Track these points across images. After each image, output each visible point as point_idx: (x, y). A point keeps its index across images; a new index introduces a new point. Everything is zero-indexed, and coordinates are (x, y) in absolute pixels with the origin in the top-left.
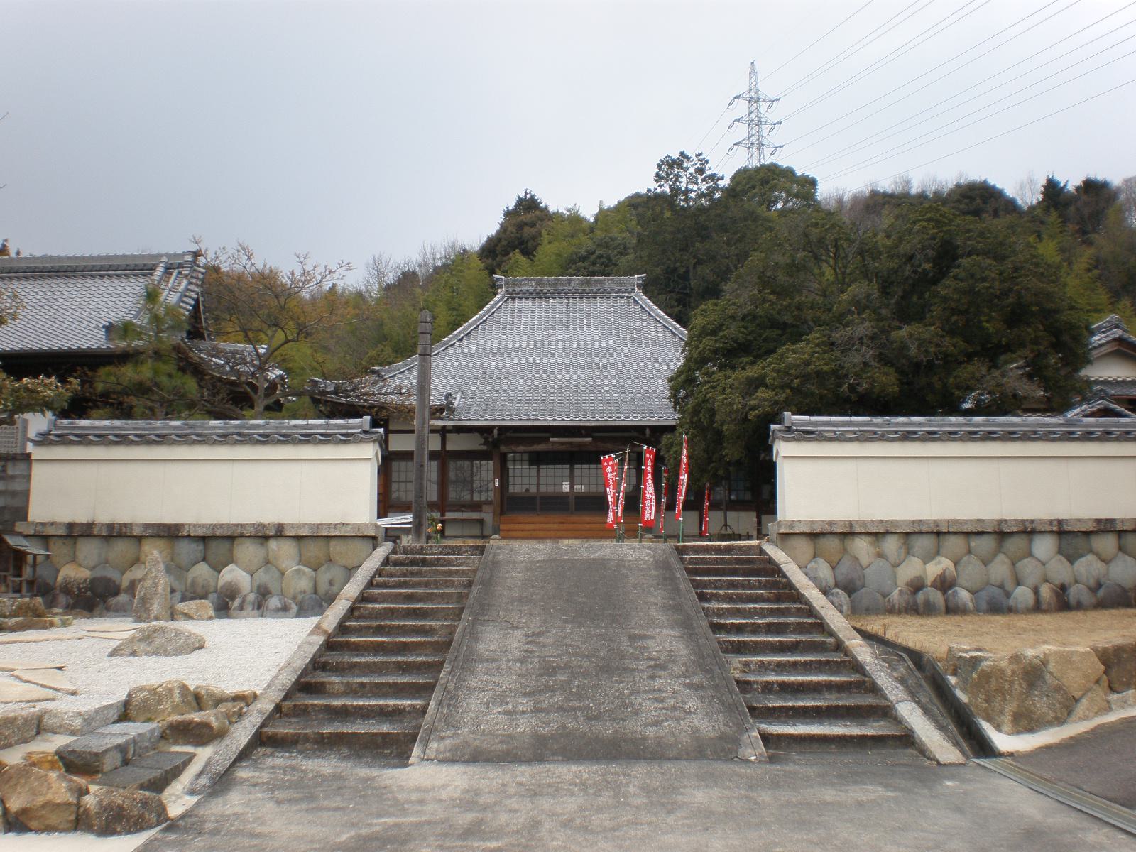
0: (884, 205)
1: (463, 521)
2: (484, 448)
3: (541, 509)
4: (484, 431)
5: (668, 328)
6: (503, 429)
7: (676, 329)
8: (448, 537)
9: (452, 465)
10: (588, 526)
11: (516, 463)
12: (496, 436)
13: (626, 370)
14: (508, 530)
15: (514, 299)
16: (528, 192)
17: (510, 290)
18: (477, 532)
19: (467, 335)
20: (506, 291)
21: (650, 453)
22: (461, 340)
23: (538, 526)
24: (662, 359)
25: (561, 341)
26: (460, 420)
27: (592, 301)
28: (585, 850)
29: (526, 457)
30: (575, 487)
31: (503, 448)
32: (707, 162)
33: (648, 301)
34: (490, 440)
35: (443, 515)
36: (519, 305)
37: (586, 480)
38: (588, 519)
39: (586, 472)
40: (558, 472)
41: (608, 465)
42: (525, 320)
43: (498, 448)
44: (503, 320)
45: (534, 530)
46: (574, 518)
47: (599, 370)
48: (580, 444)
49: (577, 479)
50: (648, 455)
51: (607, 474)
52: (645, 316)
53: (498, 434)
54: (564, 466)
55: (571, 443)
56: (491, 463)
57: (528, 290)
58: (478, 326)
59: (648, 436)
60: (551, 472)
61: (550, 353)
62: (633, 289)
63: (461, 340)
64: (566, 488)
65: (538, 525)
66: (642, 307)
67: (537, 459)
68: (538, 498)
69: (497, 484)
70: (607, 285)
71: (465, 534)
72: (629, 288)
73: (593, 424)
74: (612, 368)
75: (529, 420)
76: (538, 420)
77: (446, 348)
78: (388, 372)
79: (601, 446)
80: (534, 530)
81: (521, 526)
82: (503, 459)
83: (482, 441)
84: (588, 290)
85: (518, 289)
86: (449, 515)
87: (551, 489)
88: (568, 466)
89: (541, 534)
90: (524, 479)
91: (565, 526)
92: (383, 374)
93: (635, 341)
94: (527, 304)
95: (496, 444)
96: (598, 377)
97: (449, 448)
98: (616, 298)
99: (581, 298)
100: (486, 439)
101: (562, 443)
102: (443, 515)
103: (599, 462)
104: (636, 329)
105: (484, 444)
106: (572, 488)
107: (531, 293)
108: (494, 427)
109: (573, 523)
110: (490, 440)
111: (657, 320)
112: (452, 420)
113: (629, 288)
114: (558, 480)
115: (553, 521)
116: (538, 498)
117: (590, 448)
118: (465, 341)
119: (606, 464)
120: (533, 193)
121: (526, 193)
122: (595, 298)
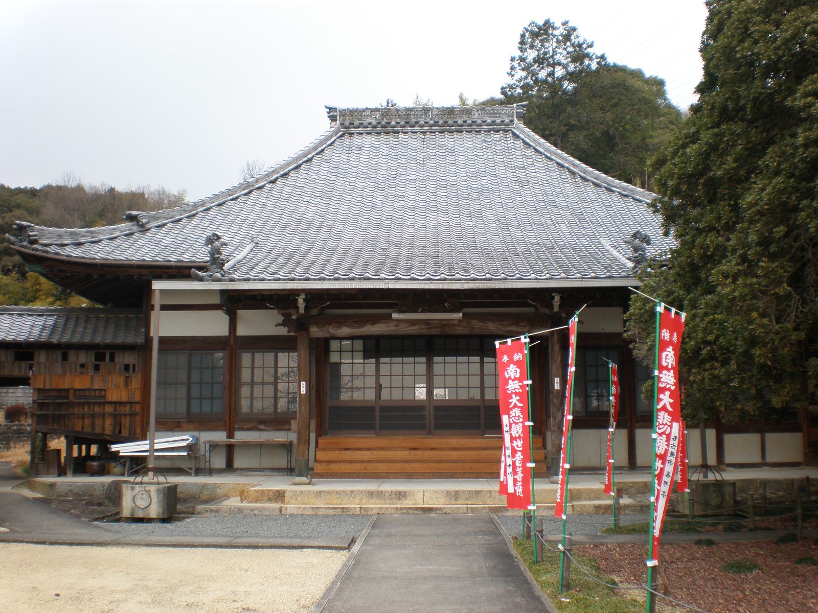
0: (699, 131)
1: (261, 446)
2: (283, 331)
3: (384, 427)
4: (280, 300)
5: (562, 166)
6: (314, 297)
7: (575, 166)
8: (238, 469)
9: (246, 358)
10: (454, 454)
11: (355, 353)
12: (302, 311)
13: (510, 215)
14: (330, 462)
15: (351, 134)
16: (390, 101)
17: (347, 123)
18: (282, 462)
19: (283, 176)
20: (342, 124)
21: (673, 325)
22: (273, 182)
23: (376, 454)
24: (561, 202)
25: (415, 181)
26: (232, 280)
27: (455, 135)
28: (438, 608)
29: (359, 344)
30: (436, 391)
31: (315, 331)
32: (574, 29)
33: (532, 133)
34: (294, 317)
35: (230, 435)
36: (357, 140)
37: (451, 381)
38: (454, 441)
39: (451, 369)
40: (409, 369)
41: (511, 361)
42: (364, 158)
43: (307, 330)
44: (335, 158)
45: (369, 461)
46: (433, 441)
47: (470, 216)
48: (443, 324)
49: (437, 380)
50: (666, 334)
51: (506, 381)
52: (530, 152)
53: (306, 308)
54: (418, 359)
55: (426, 322)
56: (294, 355)
57: (370, 123)
58: (300, 166)
59: (556, 309)
60: (397, 369)
61: (397, 195)
62: (512, 121)
63: (273, 182)
64: (421, 393)
65: (375, 453)
66: (525, 142)
67: (377, 348)
68: (377, 410)
69: (303, 391)
70: (476, 116)
71: (264, 466)
72: (507, 120)
73: (467, 286)
74: (487, 213)
75: (353, 279)
76: (369, 279)
77: (250, 192)
78: (155, 218)
79: (492, 327)
80: (369, 461)
81: (349, 455)
82: (321, 349)
83: (280, 319)
84: (450, 122)
85: (356, 123)
86: (240, 436)
87: (397, 395)
88: (424, 359)
89: (382, 467)
90: (361, 379)
91: (419, 454)
92: (144, 221)
93: (519, 181)
94: (368, 140)
95: (301, 325)
96: (468, 224)
97: (242, 331)
98: (489, 131)
99: (442, 132)
100: (287, 317)
101: (413, 322)
102: (230, 435)
103: (493, 353)
104: (519, 168)
105: (284, 324)
106: (430, 393)
107: (375, 127)
108: (295, 293)
109: (432, 449)
110: (294, 317)
111: (547, 157)
112: (219, 280)
113: (507, 120)
114: (408, 381)
115: (396, 447)
116: (377, 410)
117: (460, 330)
118: (279, 183)
119: (505, 358)
120: (394, 102)
121: (388, 103)
122: (461, 132)
